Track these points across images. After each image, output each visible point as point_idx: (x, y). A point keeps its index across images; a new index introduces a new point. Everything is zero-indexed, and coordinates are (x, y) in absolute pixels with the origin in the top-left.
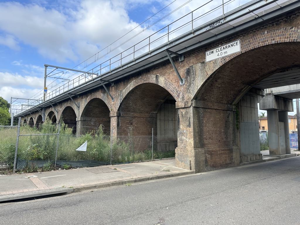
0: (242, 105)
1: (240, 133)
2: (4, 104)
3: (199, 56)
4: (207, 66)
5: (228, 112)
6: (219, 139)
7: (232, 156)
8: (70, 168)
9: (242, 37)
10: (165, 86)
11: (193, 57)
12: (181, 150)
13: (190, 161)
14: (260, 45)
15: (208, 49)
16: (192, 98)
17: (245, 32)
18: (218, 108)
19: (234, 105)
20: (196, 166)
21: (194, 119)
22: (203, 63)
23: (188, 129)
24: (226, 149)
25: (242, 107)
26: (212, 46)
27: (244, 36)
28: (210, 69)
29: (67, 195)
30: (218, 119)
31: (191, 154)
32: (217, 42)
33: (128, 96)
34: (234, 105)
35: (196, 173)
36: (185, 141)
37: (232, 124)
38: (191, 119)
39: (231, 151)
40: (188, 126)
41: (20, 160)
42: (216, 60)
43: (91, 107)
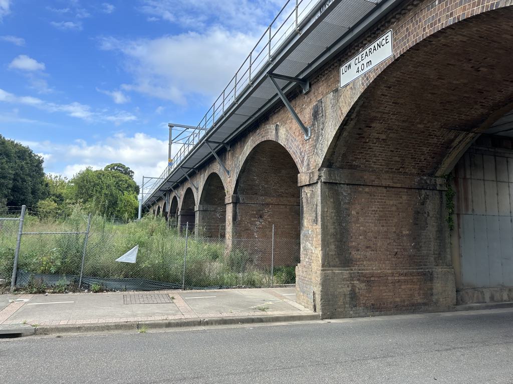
0: (468, 176)
1: (459, 237)
2: (131, 186)
3: (331, 78)
4: (342, 96)
5: (423, 192)
6: (396, 250)
7: (432, 289)
8: (101, 290)
9: (396, 23)
10: (286, 144)
11: (323, 81)
12: (303, 270)
13: (314, 294)
14: (427, 33)
16: (320, 165)
18: (391, 185)
19: (442, 177)
20: (323, 305)
21: (323, 207)
24: (413, 272)
25: (470, 181)
26: (349, 54)
27: (399, 20)
28: (346, 103)
29: (24, 338)
30: (394, 208)
33: (247, 167)
34: (442, 177)
35: (322, 319)
37: (433, 218)
39: (429, 277)
41: (23, 272)
42: (354, 82)
43: (212, 187)
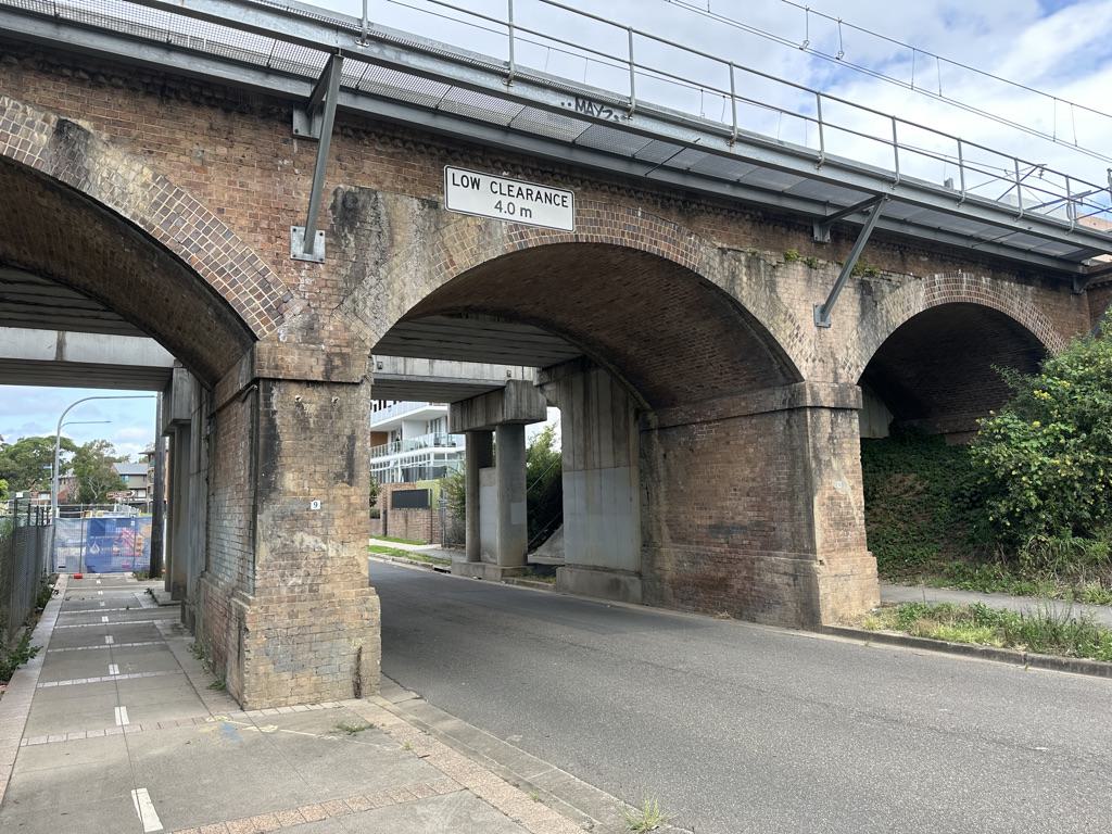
4: (451, 227)
11: (380, 153)
15: (455, 160)
17: (593, 179)
22: (434, 205)
23: (340, 490)
27: (585, 189)
31: (366, 615)
32: (502, 158)
36: (313, 555)
38: (358, 444)
40: (339, 476)
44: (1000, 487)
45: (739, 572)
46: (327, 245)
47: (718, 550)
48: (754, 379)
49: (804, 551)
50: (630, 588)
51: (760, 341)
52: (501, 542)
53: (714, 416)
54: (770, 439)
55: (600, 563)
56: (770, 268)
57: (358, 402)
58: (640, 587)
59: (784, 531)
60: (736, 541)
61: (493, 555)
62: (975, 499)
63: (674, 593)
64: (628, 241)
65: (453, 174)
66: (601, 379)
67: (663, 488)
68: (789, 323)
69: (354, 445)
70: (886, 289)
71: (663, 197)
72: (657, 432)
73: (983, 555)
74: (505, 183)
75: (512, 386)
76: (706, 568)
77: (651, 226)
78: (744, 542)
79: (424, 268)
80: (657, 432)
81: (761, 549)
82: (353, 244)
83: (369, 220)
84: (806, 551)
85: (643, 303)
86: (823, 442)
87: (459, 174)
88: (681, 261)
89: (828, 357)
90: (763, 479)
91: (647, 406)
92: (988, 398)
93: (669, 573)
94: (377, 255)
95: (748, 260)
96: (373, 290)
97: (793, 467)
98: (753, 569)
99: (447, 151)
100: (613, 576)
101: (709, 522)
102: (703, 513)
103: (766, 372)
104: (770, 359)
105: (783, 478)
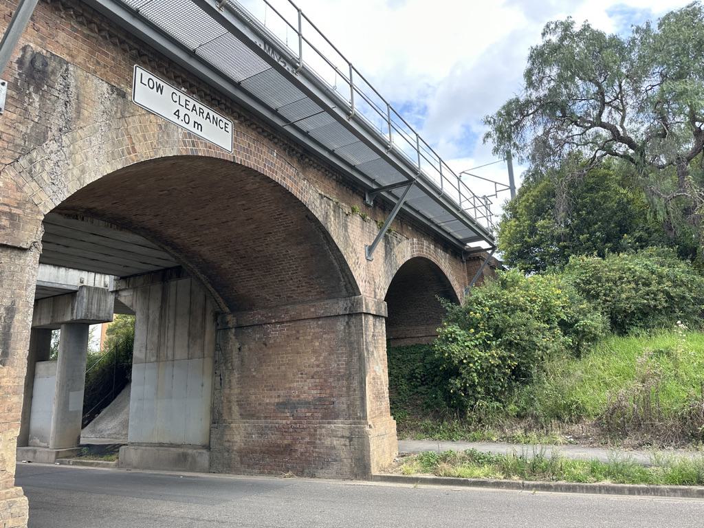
32: (184, 76)
44: (455, 372)
45: (302, 438)
46: (8, 97)
47: (284, 422)
48: (323, 292)
49: (357, 418)
50: (198, 459)
51: (336, 264)
52: (56, 427)
53: (287, 318)
54: (333, 336)
55: (166, 440)
56: (345, 215)
57: (22, 270)
58: (208, 457)
59: (341, 404)
60: (300, 415)
61: (43, 439)
62: (423, 379)
63: (241, 460)
64: (268, 173)
65: (142, 74)
66: (180, 287)
67: (236, 374)
68: (354, 254)
69: (12, 317)
70: (395, 242)
71: (290, 147)
72: (233, 330)
73: (439, 417)
74: (184, 98)
75: (85, 291)
76: (273, 437)
77: (282, 166)
78: (307, 414)
79: (107, 148)
80: (233, 330)
81: (322, 418)
82: (37, 105)
83: (58, 87)
84: (359, 418)
85: (254, 226)
86: (370, 339)
87: (147, 76)
88: (299, 196)
89: (371, 280)
90: (326, 365)
91: (227, 310)
92: (417, 318)
93: (238, 444)
94: (62, 123)
95: (334, 206)
96: (53, 156)
97: (350, 355)
98: (314, 435)
99: (139, 53)
100: (181, 450)
101: (277, 400)
102: (274, 393)
103: (333, 287)
104: (339, 277)
105: (342, 364)
